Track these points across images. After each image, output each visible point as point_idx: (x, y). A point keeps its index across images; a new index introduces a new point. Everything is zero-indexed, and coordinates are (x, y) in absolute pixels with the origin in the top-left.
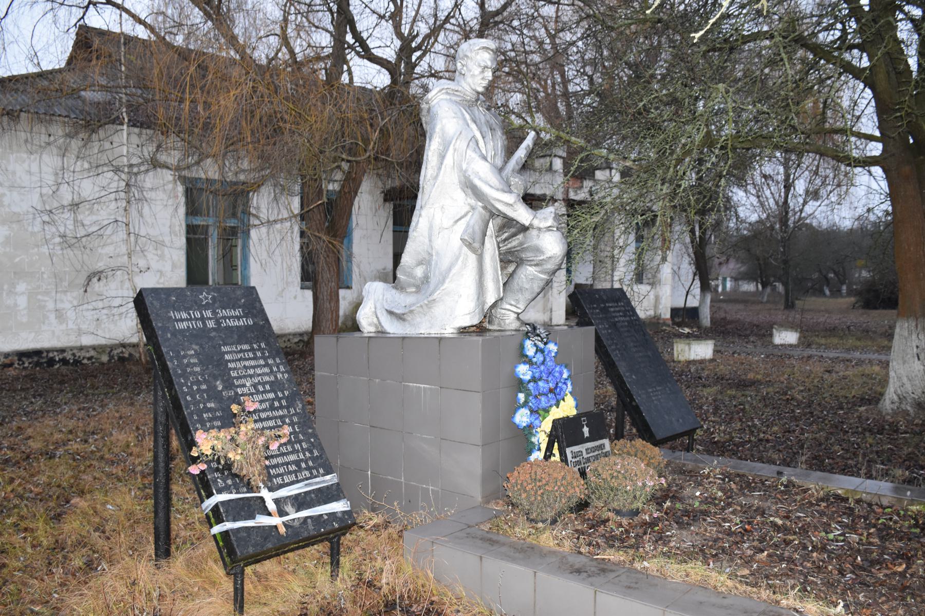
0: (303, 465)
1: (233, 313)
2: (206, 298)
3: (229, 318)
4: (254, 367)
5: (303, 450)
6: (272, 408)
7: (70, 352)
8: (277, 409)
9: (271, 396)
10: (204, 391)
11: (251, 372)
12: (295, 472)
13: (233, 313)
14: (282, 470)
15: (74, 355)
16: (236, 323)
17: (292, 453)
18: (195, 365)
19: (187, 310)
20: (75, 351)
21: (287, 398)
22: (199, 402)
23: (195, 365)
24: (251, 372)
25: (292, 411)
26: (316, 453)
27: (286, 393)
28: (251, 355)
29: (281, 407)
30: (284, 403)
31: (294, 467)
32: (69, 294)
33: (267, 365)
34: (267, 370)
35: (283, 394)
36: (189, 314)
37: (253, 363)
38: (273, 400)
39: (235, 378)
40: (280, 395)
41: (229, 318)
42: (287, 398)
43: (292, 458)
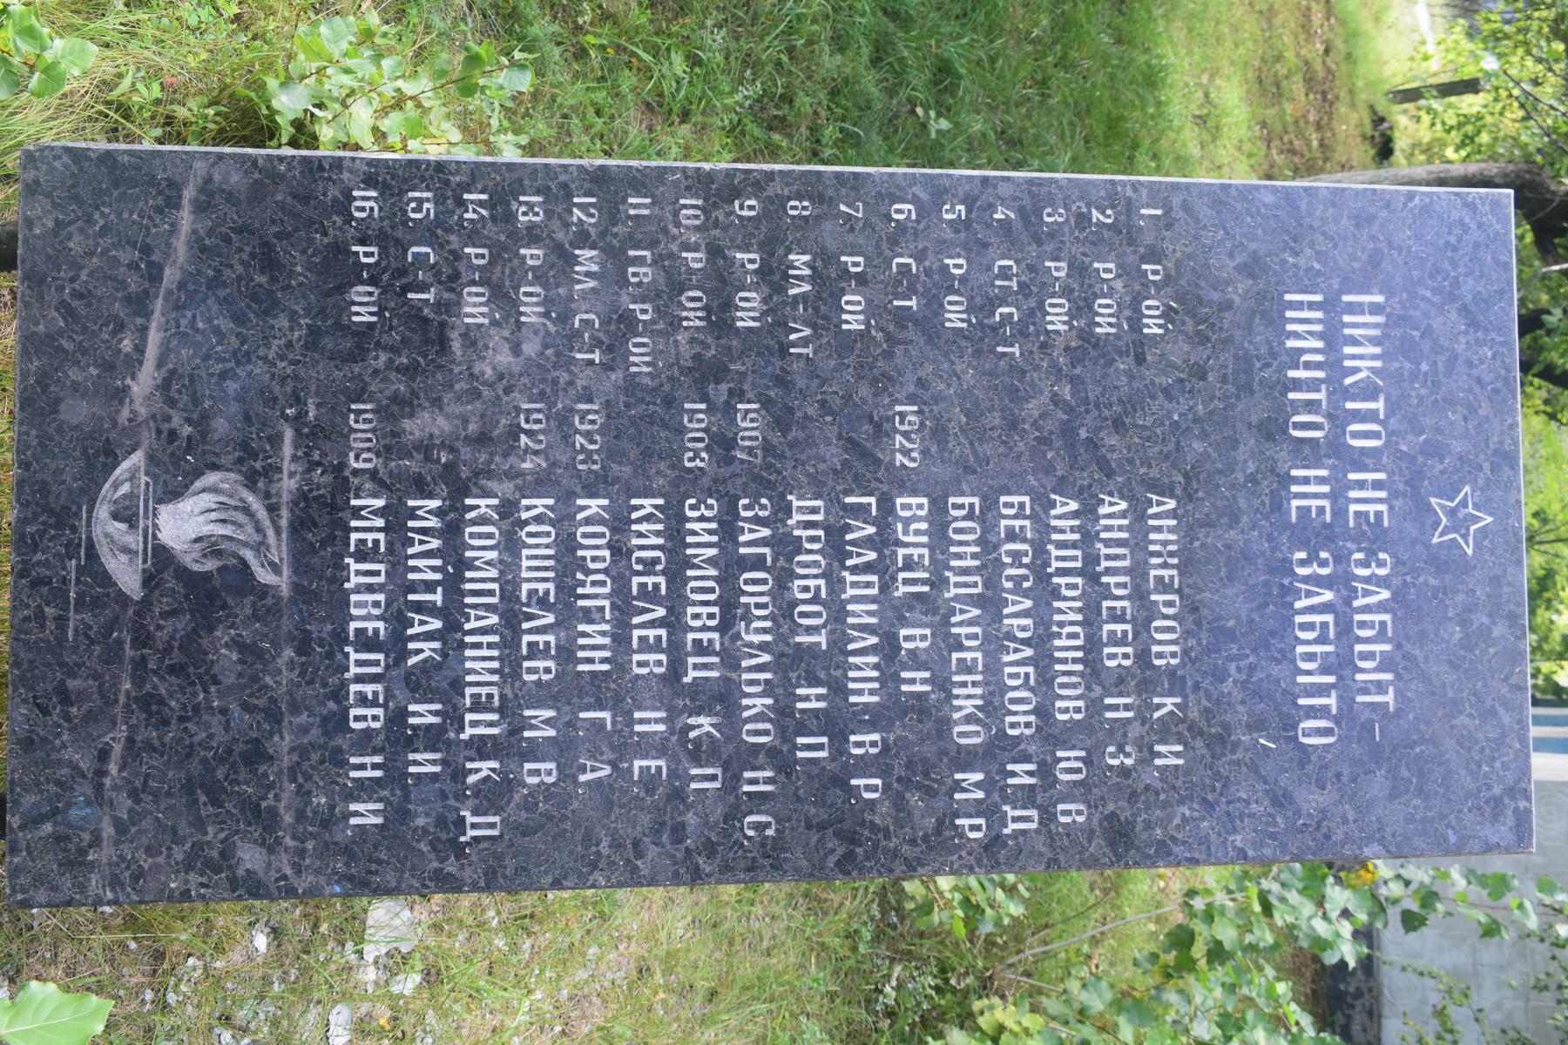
0: (424, 714)
1: (1371, 648)
2: (1459, 523)
3: (1342, 612)
4: (1042, 641)
5: (510, 747)
6: (792, 663)
7: (1364, 987)
8: (781, 692)
9: (864, 690)
10: (934, 306)
11: (1017, 618)
12: (396, 645)
13: (1371, 648)
14: (425, 569)
15: (1359, 994)
16: (1307, 646)
17: (510, 668)
18: (1082, 308)
19: (1392, 382)
20: (1367, 998)
21: (836, 778)
22: (879, 260)
23: (1082, 308)
24: (1017, 618)
25: (758, 780)
26: (479, 825)
27: (868, 786)
28: (1117, 658)
29: (787, 719)
30: (812, 748)
31: (429, 648)
32: (1520, 1004)
33: (1051, 734)
34: (1020, 720)
35: (865, 766)
36: (1369, 392)
37: (1068, 645)
38: (839, 689)
39: (990, 504)
40: (864, 742)
41: (1342, 612)
42: (836, 778)
43: (480, 667)
